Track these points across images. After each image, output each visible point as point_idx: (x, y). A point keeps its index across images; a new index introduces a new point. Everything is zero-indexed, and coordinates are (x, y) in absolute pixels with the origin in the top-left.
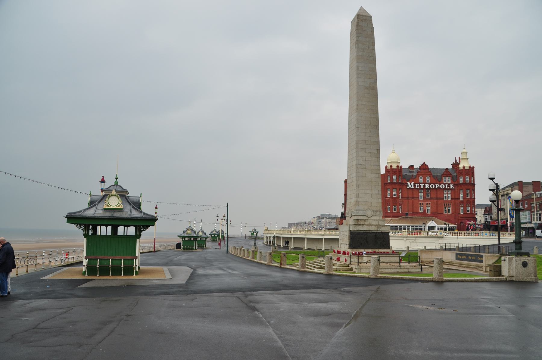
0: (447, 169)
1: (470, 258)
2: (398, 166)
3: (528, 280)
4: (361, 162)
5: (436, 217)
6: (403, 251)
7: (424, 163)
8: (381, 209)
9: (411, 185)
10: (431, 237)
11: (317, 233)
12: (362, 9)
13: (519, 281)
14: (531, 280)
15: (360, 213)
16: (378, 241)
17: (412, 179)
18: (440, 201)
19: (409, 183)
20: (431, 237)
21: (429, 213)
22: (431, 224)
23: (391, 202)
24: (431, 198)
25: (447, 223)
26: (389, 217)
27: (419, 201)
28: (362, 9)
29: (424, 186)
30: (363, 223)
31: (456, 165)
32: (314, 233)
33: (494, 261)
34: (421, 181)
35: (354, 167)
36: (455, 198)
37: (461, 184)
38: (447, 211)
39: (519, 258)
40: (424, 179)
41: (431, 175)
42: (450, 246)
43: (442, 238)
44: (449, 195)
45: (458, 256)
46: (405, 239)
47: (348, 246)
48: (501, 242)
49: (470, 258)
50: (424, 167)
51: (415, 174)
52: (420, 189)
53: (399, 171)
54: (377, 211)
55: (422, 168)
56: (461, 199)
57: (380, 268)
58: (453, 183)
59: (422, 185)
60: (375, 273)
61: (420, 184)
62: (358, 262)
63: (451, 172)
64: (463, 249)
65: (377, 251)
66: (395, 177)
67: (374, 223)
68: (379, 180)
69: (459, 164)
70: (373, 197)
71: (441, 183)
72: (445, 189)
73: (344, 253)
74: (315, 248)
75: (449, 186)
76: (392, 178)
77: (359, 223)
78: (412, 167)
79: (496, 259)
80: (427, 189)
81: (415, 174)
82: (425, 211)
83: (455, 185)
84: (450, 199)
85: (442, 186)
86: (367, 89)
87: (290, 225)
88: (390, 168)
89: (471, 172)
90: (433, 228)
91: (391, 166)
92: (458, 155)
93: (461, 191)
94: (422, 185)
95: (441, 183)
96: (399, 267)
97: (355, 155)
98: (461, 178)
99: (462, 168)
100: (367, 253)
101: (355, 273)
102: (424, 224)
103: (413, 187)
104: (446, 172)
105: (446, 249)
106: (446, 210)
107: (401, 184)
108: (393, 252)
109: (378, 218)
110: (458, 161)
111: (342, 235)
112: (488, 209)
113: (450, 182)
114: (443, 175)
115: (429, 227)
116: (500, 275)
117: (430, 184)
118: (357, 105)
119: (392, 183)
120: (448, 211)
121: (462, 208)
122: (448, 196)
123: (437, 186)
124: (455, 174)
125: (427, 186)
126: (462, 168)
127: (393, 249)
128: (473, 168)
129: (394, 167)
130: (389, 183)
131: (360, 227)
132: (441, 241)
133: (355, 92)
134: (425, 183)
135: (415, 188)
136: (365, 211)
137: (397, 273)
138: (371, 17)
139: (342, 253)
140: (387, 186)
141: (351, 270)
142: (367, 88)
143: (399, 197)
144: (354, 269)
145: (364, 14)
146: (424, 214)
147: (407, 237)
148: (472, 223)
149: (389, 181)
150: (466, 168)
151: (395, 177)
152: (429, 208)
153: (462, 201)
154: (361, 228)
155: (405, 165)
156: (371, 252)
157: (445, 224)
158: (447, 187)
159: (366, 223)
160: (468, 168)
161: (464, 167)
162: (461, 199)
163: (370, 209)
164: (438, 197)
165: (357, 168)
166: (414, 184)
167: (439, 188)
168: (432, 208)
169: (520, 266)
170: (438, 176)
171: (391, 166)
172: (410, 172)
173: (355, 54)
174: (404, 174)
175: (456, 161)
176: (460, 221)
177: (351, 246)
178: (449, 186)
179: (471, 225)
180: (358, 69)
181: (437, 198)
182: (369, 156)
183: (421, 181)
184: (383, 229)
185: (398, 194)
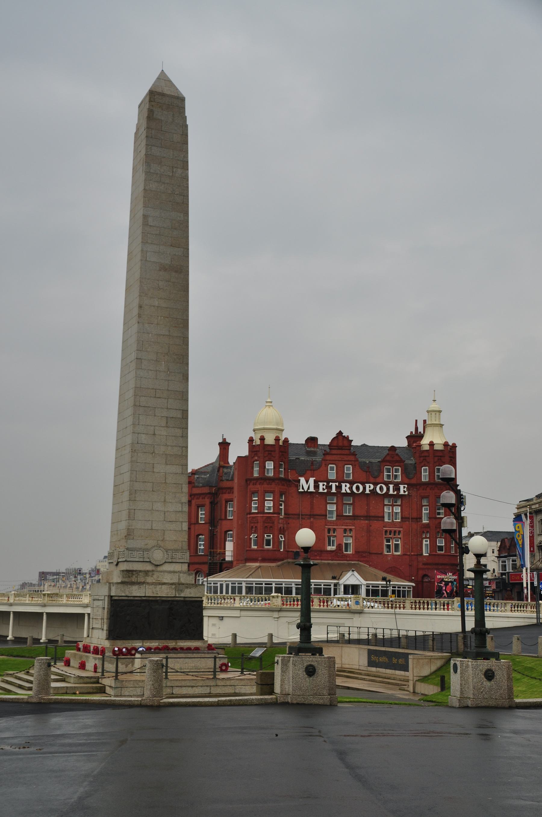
0: (393, 448)
1: (395, 661)
2: (277, 439)
3: (315, 701)
4: (143, 438)
5: (366, 562)
6: (260, 645)
7: (340, 433)
8: (185, 546)
9: (307, 484)
10: (337, 611)
11: (72, 601)
12: (163, 78)
13: (298, 704)
14: (321, 702)
15: (137, 556)
17: (309, 470)
18: (375, 525)
19: (302, 480)
20: (337, 611)
21: (350, 552)
22: (351, 578)
23: (260, 526)
24: (354, 517)
25: (389, 577)
27: (327, 523)
28: (163, 78)
29: (339, 488)
30: (141, 579)
31: (415, 438)
32: (64, 600)
33: (434, 668)
34: (332, 475)
35: (128, 449)
36: (411, 518)
37: (425, 484)
38: (393, 548)
39: (480, 662)
40: (340, 472)
41: (355, 463)
42: (359, 633)
43: (360, 612)
44: (398, 510)
45: (373, 658)
46: (276, 615)
47: (103, 634)
48: (489, 624)
49: (395, 661)
50: (341, 442)
51: (319, 459)
52: (329, 493)
53: (281, 450)
54: (176, 550)
55: (335, 444)
56: (425, 521)
57: (169, 684)
58: (407, 481)
59: (334, 485)
60: (39, 692)
61: (328, 481)
62: (117, 672)
63: (403, 456)
64: (384, 642)
65: (171, 644)
66: (270, 465)
67: (168, 580)
68: (184, 480)
69: (421, 437)
70: (170, 519)
71: (378, 480)
72: (387, 495)
73: (96, 651)
74: (59, 638)
75: (397, 488)
76: (263, 467)
77: (134, 579)
78: (312, 441)
79: (439, 663)
80: (346, 494)
81: (319, 459)
82: (339, 546)
83: (410, 487)
85: (381, 488)
86: (165, 270)
87: (43, 576)
88: (258, 442)
89: (449, 454)
90: (354, 589)
91: (262, 439)
92: (422, 416)
93: (425, 502)
94: (334, 485)
95: (378, 480)
96: (212, 683)
97: (130, 421)
98: (425, 470)
99: (427, 448)
100: (149, 649)
101: (110, 696)
102: (334, 578)
103: (312, 489)
104: (392, 455)
105: (350, 642)
106: (388, 547)
107: (286, 481)
108: (210, 647)
109: (177, 567)
110: (421, 430)
111: (90, 604)
112: (508, 544)
113: (399, 480)
114: (384, 461)
115: (346, 587)
116: (272, 692)
117: (352, 483)
118: (140, 307)
119: (263, 479)
120: (395, 548)
121: (426, 542)
122: (392, 512)
123: (369, 487)
124: (412, 461)
125: (346, 488)
126: (427, 448)
127: (211, 641)
128: (454, 446)
129: (270, 440)
130: (257, 479)
131: (135, 588)
132: (357, 621)
133: (137, 275)
134: (340, 481)
135: (317, 493)
136: (148, 550)
137: (210, 695)
138: (182, 100)
139: (92, 649)
140: (252, 487)
141: (102, 690)
142: (163, 268)
143: (279, 513)
144: (108, 690)
145: (167, 91)
146: (338, 553)
147: (280, 610)
148: (450, 577)
149: (256, 475)
150: (436, 447)
151: (270, 465)
152: (350, 541)
153: (427, 526)
154: (136, 592)
155: (297, 437)
156: (157, 648)
157: (384, 579)
158: (391, 492)
159: (149, 580)
160: (441, 448)
161: (431, 444)
162: (425, 521)
163: (159, 547)
164: (372, 514)
165: (133, 451)
167: (373, 492)
168: (356, 541)
169: (302, 673)
170: (372, 463)
171: (262, 439)
172: (309, 453)
173: (141, 188)
174: (293, 458)
175: (417, 429)
176: (421, 573)
178: (397, 488)
179: (447, 583)
180: (145, 223)
181: (368, 517)
182: (163, 423)
183: (332, 475)
184: (189, 593)
185: (276, 505)
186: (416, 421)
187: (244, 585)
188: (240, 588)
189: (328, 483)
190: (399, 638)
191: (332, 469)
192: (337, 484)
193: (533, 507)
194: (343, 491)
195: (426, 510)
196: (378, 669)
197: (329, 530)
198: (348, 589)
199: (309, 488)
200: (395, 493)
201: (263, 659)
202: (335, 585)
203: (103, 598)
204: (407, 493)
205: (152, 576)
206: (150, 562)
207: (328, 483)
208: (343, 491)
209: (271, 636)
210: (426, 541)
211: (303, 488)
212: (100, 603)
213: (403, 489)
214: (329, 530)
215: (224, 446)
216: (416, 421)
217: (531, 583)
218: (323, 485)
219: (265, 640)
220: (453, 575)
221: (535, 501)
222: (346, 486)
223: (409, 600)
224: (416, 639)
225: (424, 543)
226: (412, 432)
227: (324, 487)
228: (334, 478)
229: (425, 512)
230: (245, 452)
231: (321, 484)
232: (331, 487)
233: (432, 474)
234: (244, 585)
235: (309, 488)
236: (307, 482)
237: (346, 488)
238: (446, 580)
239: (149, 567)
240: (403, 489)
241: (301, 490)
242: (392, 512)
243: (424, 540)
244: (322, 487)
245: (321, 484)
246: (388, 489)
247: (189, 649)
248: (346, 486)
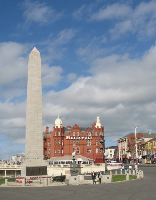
16: (42, 171)
19: (67, 136)
24: (80, 145)
26: (56, 156)
34: (74, 135)
37: (96, 136)
45: (86, 178)
46: (62, 169)
56: (97, 145)
59: (75, 137)
67: (41, 162)
84: (90, 145)
85: (86, 138)
94: (75, 137)
103: (69, 138)
106: (88, 152)
113: (90, 135)
119: (57, 136)
122: (90, 143)
123: (83, 138)
125: (77, 138)
126: (96, 127)
134: (76, 136)
147: (63, 168)
153: (97, 146)
156: (2, 180)
161: (98, 127)
166: (70, 137)
167: (84, 139)
169: (107, 178)
177: (27, 175)
181: (83, 145)
183: (74, 135)
187: (54, 162)
188: (53, 163)
190: (80, 168)
191: (74, 133)
196: (122, 181)
209: (61, 174)
212: (24, 168)
215: (47, 128)
219: (60, 175)
223: (93, 164)
228: (75, 135)
230: (53, 130)
231: (71, 137)
233: (98, 134)
234: (54, 162)
236: (68, 137)
240: (91, 138)
242: (90, 143)
244: (72, 138)
247: (36, 178)
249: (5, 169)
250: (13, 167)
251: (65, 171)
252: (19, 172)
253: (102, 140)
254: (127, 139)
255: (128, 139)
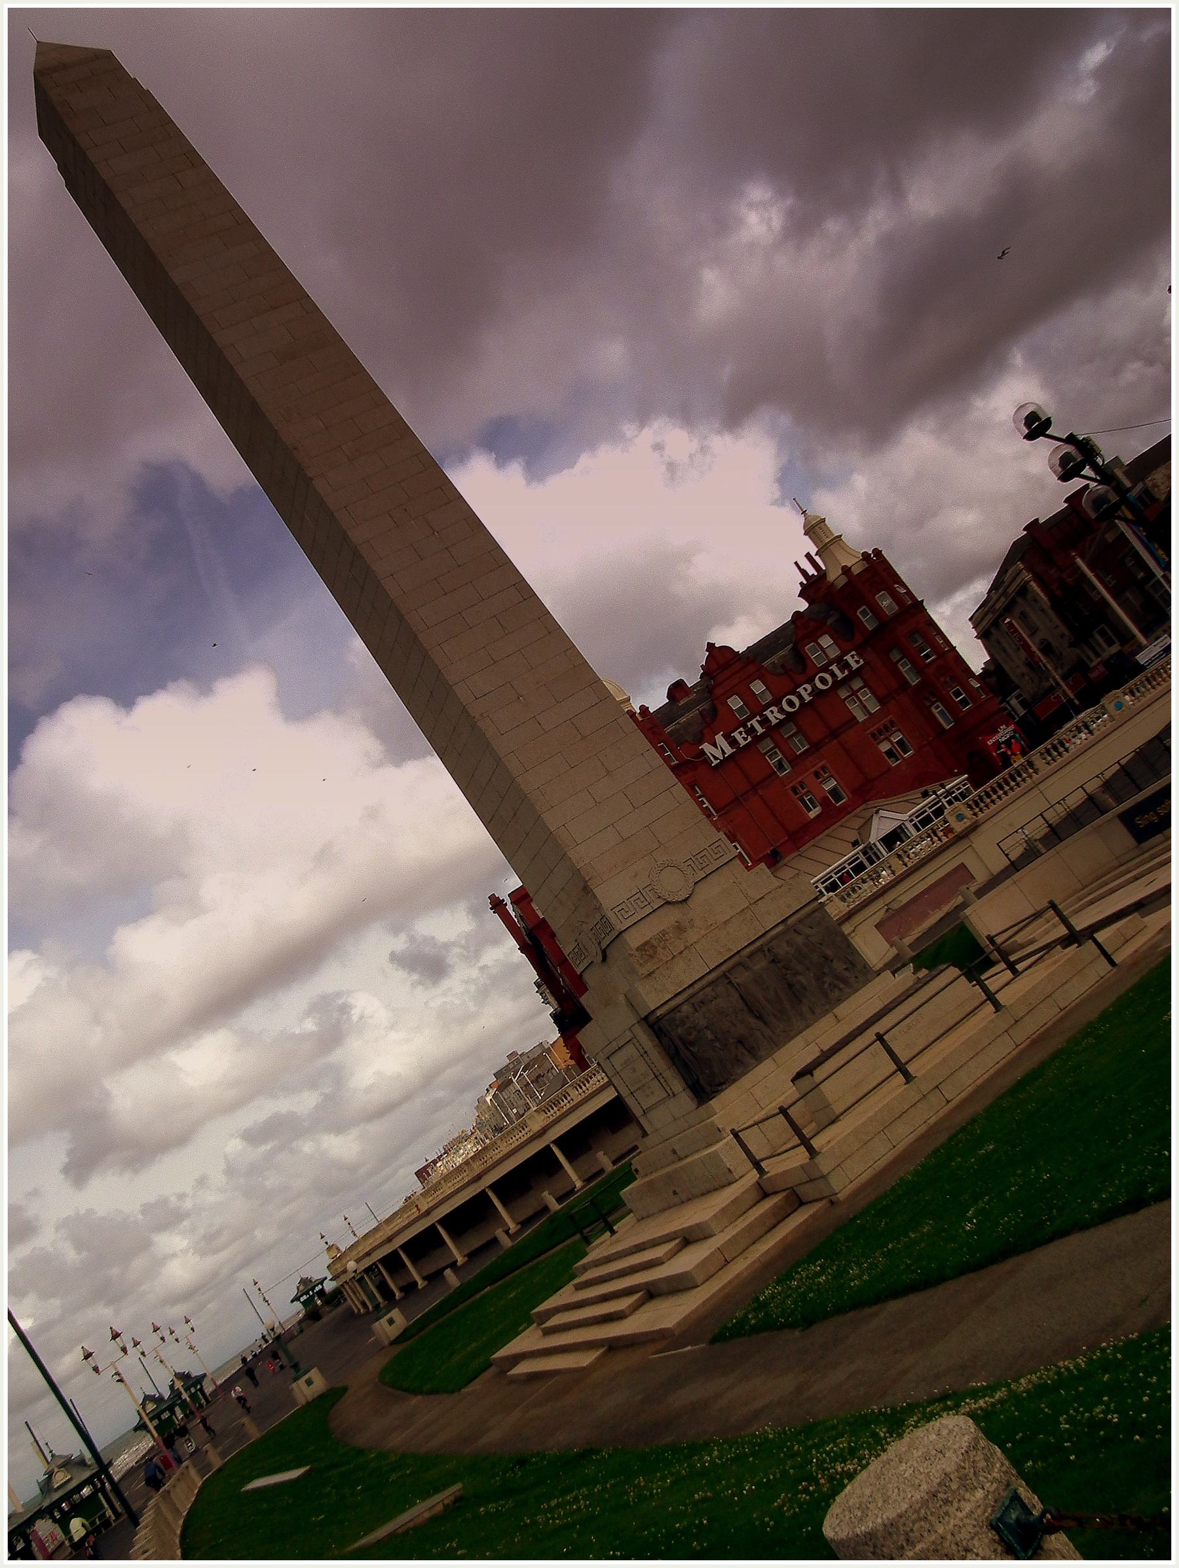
19: (706, 747)
24: (815, 747)
29: (765, 722)
45: (1141, 822)
52: (758, 739)
56: (914, 681)
59: (754, 723)
72: (837, 684)
78: (677, 689)
80: (781, 723)
82: (825, 803)
93: (895, 656)
99: (843, 580)
103: (729, 751)
110: (811, 571)
113: (834, 653)
117: (777, 702)
122: (863, 705)
123: (805, 691)
125: (774, 715)
135: (740, 751)
150: (856, 571)
158: (840, 676)
161: (846, 571)
162: (914, 681)
167: (816, 693)
178: (845, 666)
179: (1008, 743)
181: (833, 734)
186: (796, 563)
189: (745, 726)
192: (758, 718)
193: (997, 607)
194: (774, 721)
195: (904, 665)
197: (794, 790)
198: (890, 840)
199: (724, 752)
200: (846, 672)
201: (1056, 902)
202: (865, 852)
203: (629, 1035)
204: (862, 662)
205: (692, 926)
206: (668, 903)
207: (745, 726)
208: (774, 721)
210: (937, 707)
211: (716, 758)
213: (852, 660)
214: (794, 790)
216: (796, 563)
217: (378, 1288)
218: (740, 733)
220: (1007, 726)
221: (995, 597)
222: (772, 712)
224: (1128, 774)
225: (935, 712)
226: (801, 583)
227: (744, 735)
229: (905, 669)
231: (736, 734)
232: (753, 729)
235: (724, 752)
236: (715, 745)
237: (774, 715)
238: (1004, 739)
239: (671, 916)
240: (852, 660)
241: (715, 762)
243: (933, 709)
244: (740, 737)
245: (736, 734)
246: (833, 674)
248: (772, 712)
249: (479, 1177)
250: (522, 1136)
251: (877, 926)
252: (615, 1116)
253: (118, 1378)
254: (1027, 576)
255: (1030, 569)
